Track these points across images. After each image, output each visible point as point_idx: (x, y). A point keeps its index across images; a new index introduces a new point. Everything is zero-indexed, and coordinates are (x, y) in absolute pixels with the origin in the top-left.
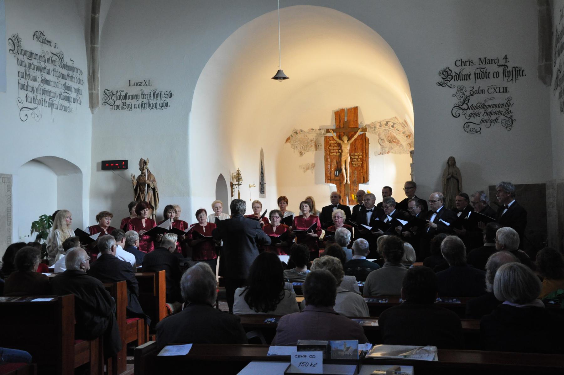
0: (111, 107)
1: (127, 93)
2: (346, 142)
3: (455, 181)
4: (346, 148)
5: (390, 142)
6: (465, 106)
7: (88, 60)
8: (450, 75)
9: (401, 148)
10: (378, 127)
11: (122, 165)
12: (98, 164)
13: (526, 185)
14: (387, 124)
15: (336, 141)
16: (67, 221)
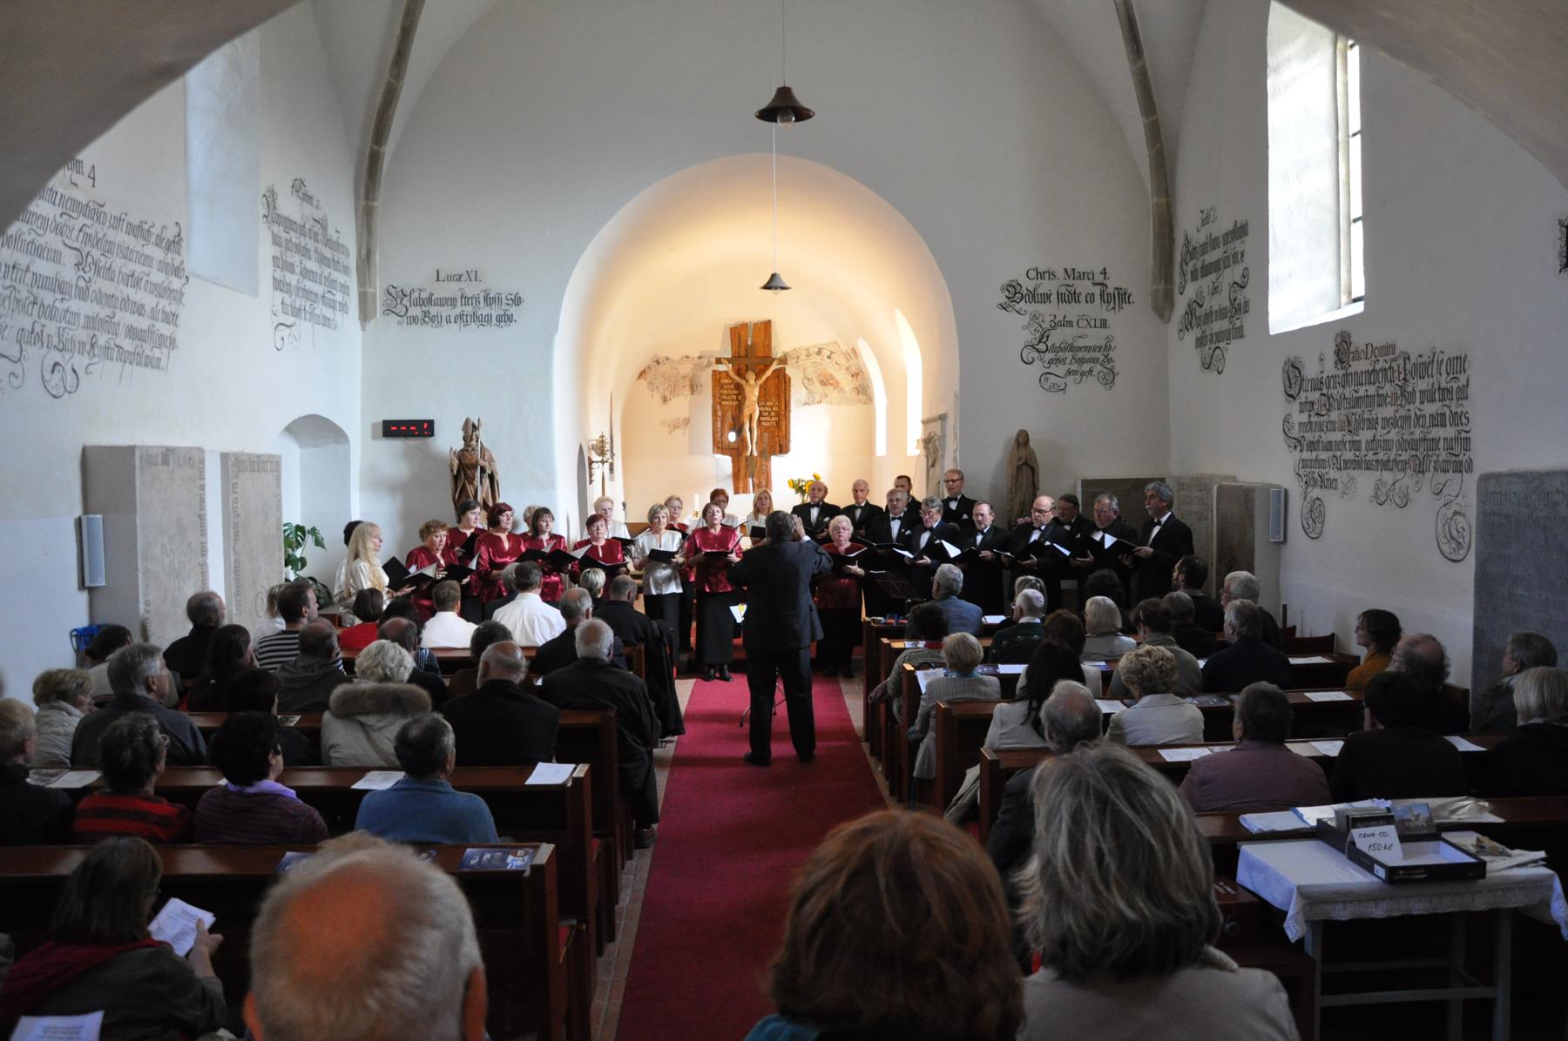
0: (399, 318)
1: (432, 294)
2: (752, 382)
3: (1029, 471)
4: (753, 393)
5: (823, 383)
6: (1042, 347)
7: (357, 231)
8: (1019, 293)
9: (842, 395)
10: (803, 357)
11: (424, 429)
12: (374, 425)
13: (1137, 479)
14: (819, 352)
15: (733, 380)
16: (374, 543)
